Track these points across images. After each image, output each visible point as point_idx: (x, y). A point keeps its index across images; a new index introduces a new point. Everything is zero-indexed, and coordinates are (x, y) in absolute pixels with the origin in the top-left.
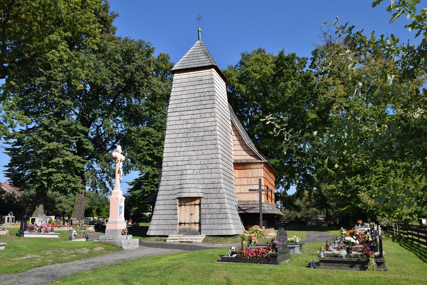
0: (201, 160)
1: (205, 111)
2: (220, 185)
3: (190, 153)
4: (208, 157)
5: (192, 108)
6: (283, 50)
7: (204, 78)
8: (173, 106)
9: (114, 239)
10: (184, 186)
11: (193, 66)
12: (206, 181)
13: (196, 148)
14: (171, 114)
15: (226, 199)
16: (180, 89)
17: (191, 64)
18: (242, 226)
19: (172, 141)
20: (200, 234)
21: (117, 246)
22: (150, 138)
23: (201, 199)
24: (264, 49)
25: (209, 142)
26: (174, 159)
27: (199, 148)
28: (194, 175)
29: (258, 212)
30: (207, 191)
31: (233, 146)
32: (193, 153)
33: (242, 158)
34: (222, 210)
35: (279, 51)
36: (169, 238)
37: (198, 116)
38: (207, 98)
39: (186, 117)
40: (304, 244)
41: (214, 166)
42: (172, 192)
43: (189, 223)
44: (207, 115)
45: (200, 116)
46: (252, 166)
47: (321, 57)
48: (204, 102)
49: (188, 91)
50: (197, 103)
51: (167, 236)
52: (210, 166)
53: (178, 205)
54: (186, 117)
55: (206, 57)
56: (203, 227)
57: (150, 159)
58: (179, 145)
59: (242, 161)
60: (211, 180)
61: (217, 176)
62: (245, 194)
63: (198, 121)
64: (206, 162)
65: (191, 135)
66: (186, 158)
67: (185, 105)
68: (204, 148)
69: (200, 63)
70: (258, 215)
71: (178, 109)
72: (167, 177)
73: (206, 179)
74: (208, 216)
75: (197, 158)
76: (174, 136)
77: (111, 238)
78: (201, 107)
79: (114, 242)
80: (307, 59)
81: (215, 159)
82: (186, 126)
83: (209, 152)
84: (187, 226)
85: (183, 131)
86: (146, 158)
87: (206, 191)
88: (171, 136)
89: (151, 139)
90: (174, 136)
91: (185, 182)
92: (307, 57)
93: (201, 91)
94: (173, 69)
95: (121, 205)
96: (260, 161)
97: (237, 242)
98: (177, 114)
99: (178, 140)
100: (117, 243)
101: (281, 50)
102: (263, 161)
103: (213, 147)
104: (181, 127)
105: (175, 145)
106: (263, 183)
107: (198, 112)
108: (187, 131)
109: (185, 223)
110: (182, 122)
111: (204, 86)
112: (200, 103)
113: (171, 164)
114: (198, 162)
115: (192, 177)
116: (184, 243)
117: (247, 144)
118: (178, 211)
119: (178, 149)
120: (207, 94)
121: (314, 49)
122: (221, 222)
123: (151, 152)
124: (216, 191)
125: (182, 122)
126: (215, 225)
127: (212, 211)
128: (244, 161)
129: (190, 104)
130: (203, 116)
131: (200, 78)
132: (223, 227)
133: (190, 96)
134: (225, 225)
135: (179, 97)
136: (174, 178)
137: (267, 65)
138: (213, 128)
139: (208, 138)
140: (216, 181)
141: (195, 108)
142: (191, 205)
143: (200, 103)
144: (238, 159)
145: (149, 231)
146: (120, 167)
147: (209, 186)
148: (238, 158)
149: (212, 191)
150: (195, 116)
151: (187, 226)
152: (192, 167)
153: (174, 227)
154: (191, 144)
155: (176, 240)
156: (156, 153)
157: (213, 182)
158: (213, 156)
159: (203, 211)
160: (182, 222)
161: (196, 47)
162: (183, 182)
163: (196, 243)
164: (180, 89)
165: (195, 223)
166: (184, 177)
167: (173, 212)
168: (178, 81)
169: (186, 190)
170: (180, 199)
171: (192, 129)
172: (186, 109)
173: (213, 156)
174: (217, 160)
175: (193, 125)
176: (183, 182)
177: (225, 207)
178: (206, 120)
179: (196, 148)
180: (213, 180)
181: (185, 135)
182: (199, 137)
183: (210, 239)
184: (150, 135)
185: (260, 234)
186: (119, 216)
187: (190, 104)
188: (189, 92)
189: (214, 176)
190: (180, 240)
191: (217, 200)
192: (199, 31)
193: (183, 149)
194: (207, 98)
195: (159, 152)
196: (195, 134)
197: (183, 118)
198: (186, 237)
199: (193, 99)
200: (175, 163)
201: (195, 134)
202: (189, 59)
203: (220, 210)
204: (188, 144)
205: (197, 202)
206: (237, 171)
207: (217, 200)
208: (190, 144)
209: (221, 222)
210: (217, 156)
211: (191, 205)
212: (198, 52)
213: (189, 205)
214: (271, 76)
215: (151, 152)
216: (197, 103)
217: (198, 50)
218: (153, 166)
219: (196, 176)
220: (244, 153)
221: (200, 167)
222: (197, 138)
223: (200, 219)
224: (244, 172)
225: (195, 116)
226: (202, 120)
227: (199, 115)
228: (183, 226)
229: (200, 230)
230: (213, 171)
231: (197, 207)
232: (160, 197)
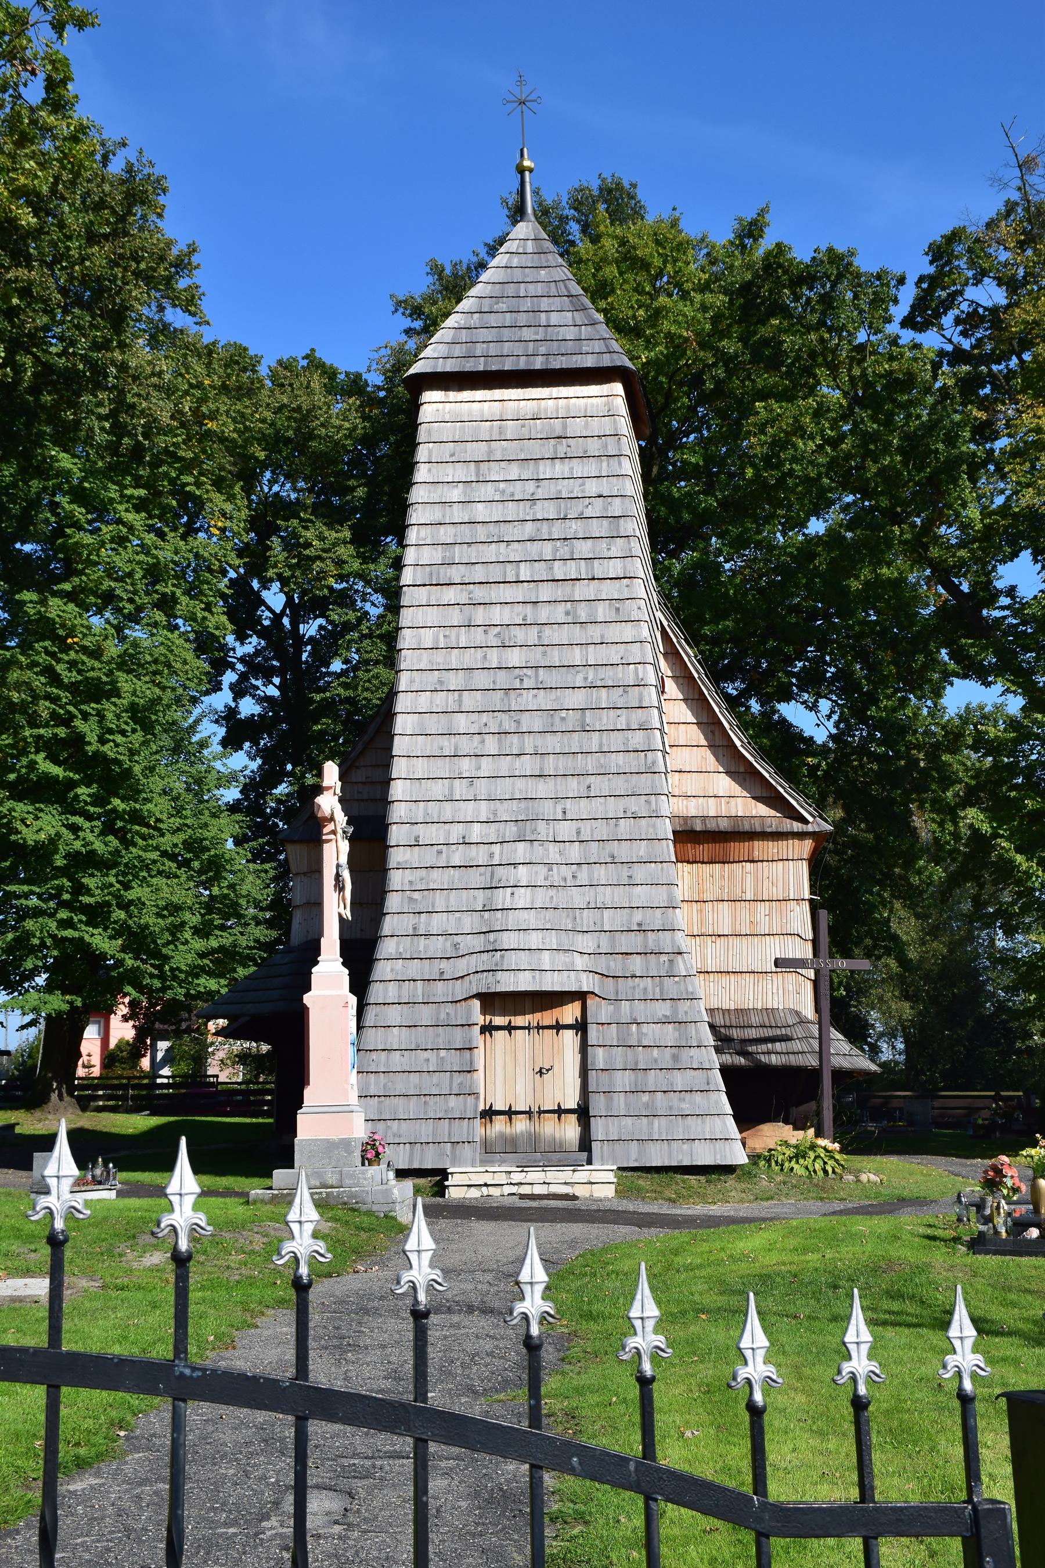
0: (580, 823)
1: (588, 590)
2: (673, 940)
4: (614, 808)
5: (525, 572)
6: (762, 213)
7: (576, 427)
8: (428, 555)
9: (347, 1182)
10: (508, 940)
11: (522, 364)
12: (610, 920)
13: (550, 765)
14: (420, 595)
16: (460, 473)
19: (433, 724)
20: (589, 1162)
21: (369, 1213)
22: (53, 655)
23: (589, 1002)
24: (634, 186)
25: (615, 741)
26: (448, 811)
29: (812, 1061)
30: (615, 965)
33: (711, 808)
34: (686, 1053)
35: (740, 220)
37: (559, 613)
38: (598, 528)
39: (498, 615)
42: (444, 964)
43: (529, 1113)
44: (602, 612)
45: (567, 613)
46: (760, 848)
47: (975, 277)
48: (584, 548)
49: (502, 485)
50: (547, 550)
52: (624, 852)
53: (477, 1029)
54: (498, 615)
55: (579, 317)
56: (599, 1129)
57: (57, 771)
58: (467, 745)
59: (711, 826)
60: (631, 915)
61: (659, 896)
62: (725, 979)
64: (602, 830)
65: (527, 700)
66: (505, 811)
67: (491, 552)
68: (590, 764)
70: (814, 1074)
71: (455, 574)
72: (416, 895)
73: (606, 912)
74: (623, 1080)
75: (559, 811)
76: (441, 701)
77: (332, 1179)
78: (571, 570)
79: (353, 1195)
80: (901, 281)
81: (643, 821)
83: (620, 785)
84: (521, 1125)
85: (482, 680)
86: (32, 765)
87: (612, 964)
88: (424, 701)
89: (59, 661)
90: (441, 701)
92: (897, 271)
94: (415, 369)
96: (797, 826)
97: (772, 1198)
98: (450, 595)
99: (462, 723)
100: (369, 1199)
101: (750, 215)
102: (810, 828)
103: (634, 762)
104: (471, 658)
105: (448, 745)
107: (560, 592)
108: (503, 679)
109: (510, 1113)
110: (478, 636)
111: (579, 468)
112: (564, 551)
113: (429, 834)
115: (542, 898)
116: (545, 1202)
118: (479, 1055)
119: (466, 766)
120: (596, 508)
121: (937, 232)
122: (684, 1106)
123: (62, 732)
125: (478, 636)
126: (656, 1120)
127: (641, 1058)
128: (724, 825)
129: (515, 552)
130: (583, 614)
131: (557, 425)
133: (511, 511)
134: (703, 1123)
135: (458, 514)
136: (455, 900)
137: (685, 296)
138: (632, 676)
139: (607, 719)
140: (656, 919)
141: (540, 571)
142: (539, 1028)
143: (564, 551)
144: (692, 812)
147: (626, 942)
148: (691, 808)
149: (637, 964)
150: (544, 614)
151: (521, 1125)
152: (538, 852)
153: (460, 1131)
156: (92, 737)
157: (639, 925)
158: (635, 805)
159: (599, 1057)
160: (498, 1107)
161: (515, 261)
162: (498, 920)
163: (592, 1199)
164: (460, 473)
165: (560, 1112)
166: (502, 898)
167: (454, 1060)
168: (447, 432)
170: (491, 1001)
171: (529, 672)
172: (495, 573)
173: (635, 805)
174: (654, 826)
175: (535, 656)
176: (498, 920)
177: (699, 1040)
178: (595, 633)
180: (638, 916)
181: (496, 700)
182: (564, 714)
183: (644, 1182)
184: (55, 638)
185: (831, 1162)
187: (515, 552)
188: (503, 492)
189: (641, 895)
190: (514, 1189)
191: (663, 1009)
193: (487, 766)
194: (598, 528)
195: (111, 731)
196: (544, 700)
197: (480, 616)
198: (535, 1175)
199: (529, 529)
200: (456, 832)
201: (544, 700)
202: (493, 320)
204: (514, 743)
205: (570, 1013)
206: (687, 867)
207: (663, 1009)
209: (686, 1108)
210: (654, 806)
211: (539, 1028)
212: (532, 289)
213: (528, 1028)
214: (714, 365)
215: (62, 732)
216: (547, 550)
217: (531, 275)
218: (70, 808)
219: (561, 898)
220: (725, 784)
221: (575, 852)
222: (557, 720)
223: (585, 1091)
224: (717, 875)
225: (544, 614)
226: (577, 634)
227: (561, 608)
228: (499, 1125)
229: (585, 1144)
230: (640, 873)
231: (570, 1037)
232: (386, 990)
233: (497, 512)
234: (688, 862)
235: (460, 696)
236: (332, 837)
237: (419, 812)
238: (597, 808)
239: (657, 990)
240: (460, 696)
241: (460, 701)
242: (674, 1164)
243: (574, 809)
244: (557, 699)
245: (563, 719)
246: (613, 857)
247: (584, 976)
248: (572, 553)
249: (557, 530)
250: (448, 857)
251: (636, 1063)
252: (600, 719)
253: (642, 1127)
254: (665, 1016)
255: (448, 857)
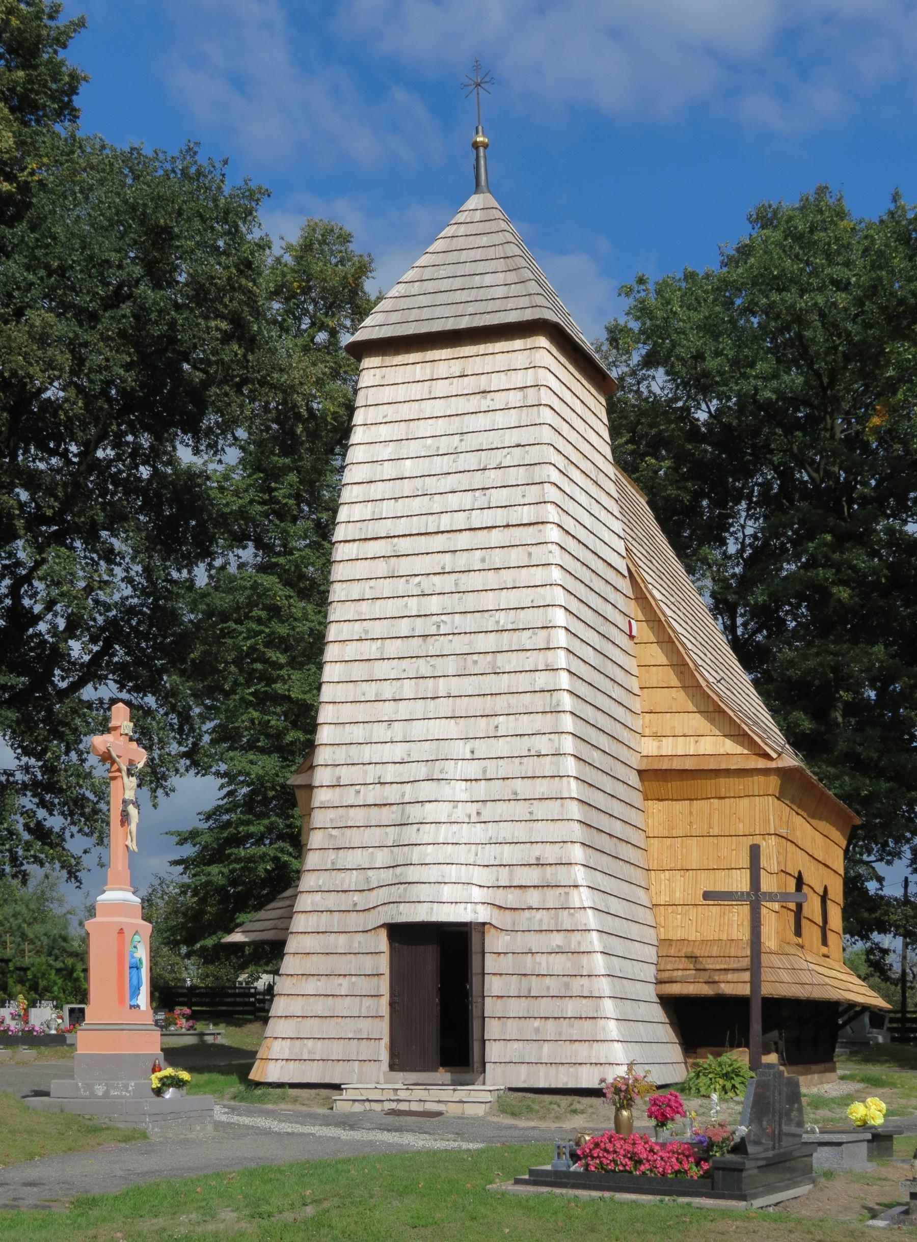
3: (437, 728)
10: (412, 874)
13: (462, 707)
15: (594, 935)
17: (438, 312)
18: (675, 1052)
25: (522, 682)
27: (477, 705)
28: (455, 827)
29: (745, 990)
30: (511, 898)
31: (637, 691)
32: (452, 729)
33: (681, 747)
36: (345, 1095)
40: (900, 1133)
41: (541, 788)
42: (356, 897)
48: (499, 497)
49: (429, 441)
51: (337, 1087)
63: (474, 581)
67: (416, 505)
69: (481, 307)
70: (741, 1003)
72: (335, 832)
75: (492, 728)
82: (419, 604)
87: (510, 896)
91: (416, 854)
93: (485, 440)
95: (137, 955)
96: (761, 763)
102: (773, 765)
103: (539, 703)
106: (769, 861)
112: (482, 501)
113: (347, 775)
114: (472, 769)
117: (703, 684)
124: (552, 898)
127: (534, 985)
128: (689, 765)
132: (582, 1052)
135: (388, 470)
145: (257, 1062)
146: (127, 797)
149: (533, 898)
154: (442, 686)
155: (377, 1107)
157: (538, 859)
162: (401, 855)
166: (410, 835)
169: (423, 892)
179: (462, 707)
180: (537, 850)
182: (475, 657)
186: (128, 1003)
190: (393, 1105)
191: (557, 940)
192: (476, 145)
193: (404, 710)
194: (513, 475)
203: (565, 979)
207: (557, 940)
208: (436, 688)
220: (698, 722)
221: (481, 790)
226: (492, 580)
233: (423, 466)
234: (658, 800)
235: (383, 644)
236: (117, 774)
237: (340, 755)
238: (502, 747)
239: (552, 922)
240: (383, 644)
241: (382, 649)
242: (560, 1086)
243: (482, 749)
244: (470, 643)
245: (475, 662)
246: (516, 794)
247: (480, 908)
248: (489, 502)
249: (478, 480)
250: (365, 796)
251: (529, 991)
252: (510, 662)
253: (530, 1052)
254: (558, 946)
255: (365, 796)
